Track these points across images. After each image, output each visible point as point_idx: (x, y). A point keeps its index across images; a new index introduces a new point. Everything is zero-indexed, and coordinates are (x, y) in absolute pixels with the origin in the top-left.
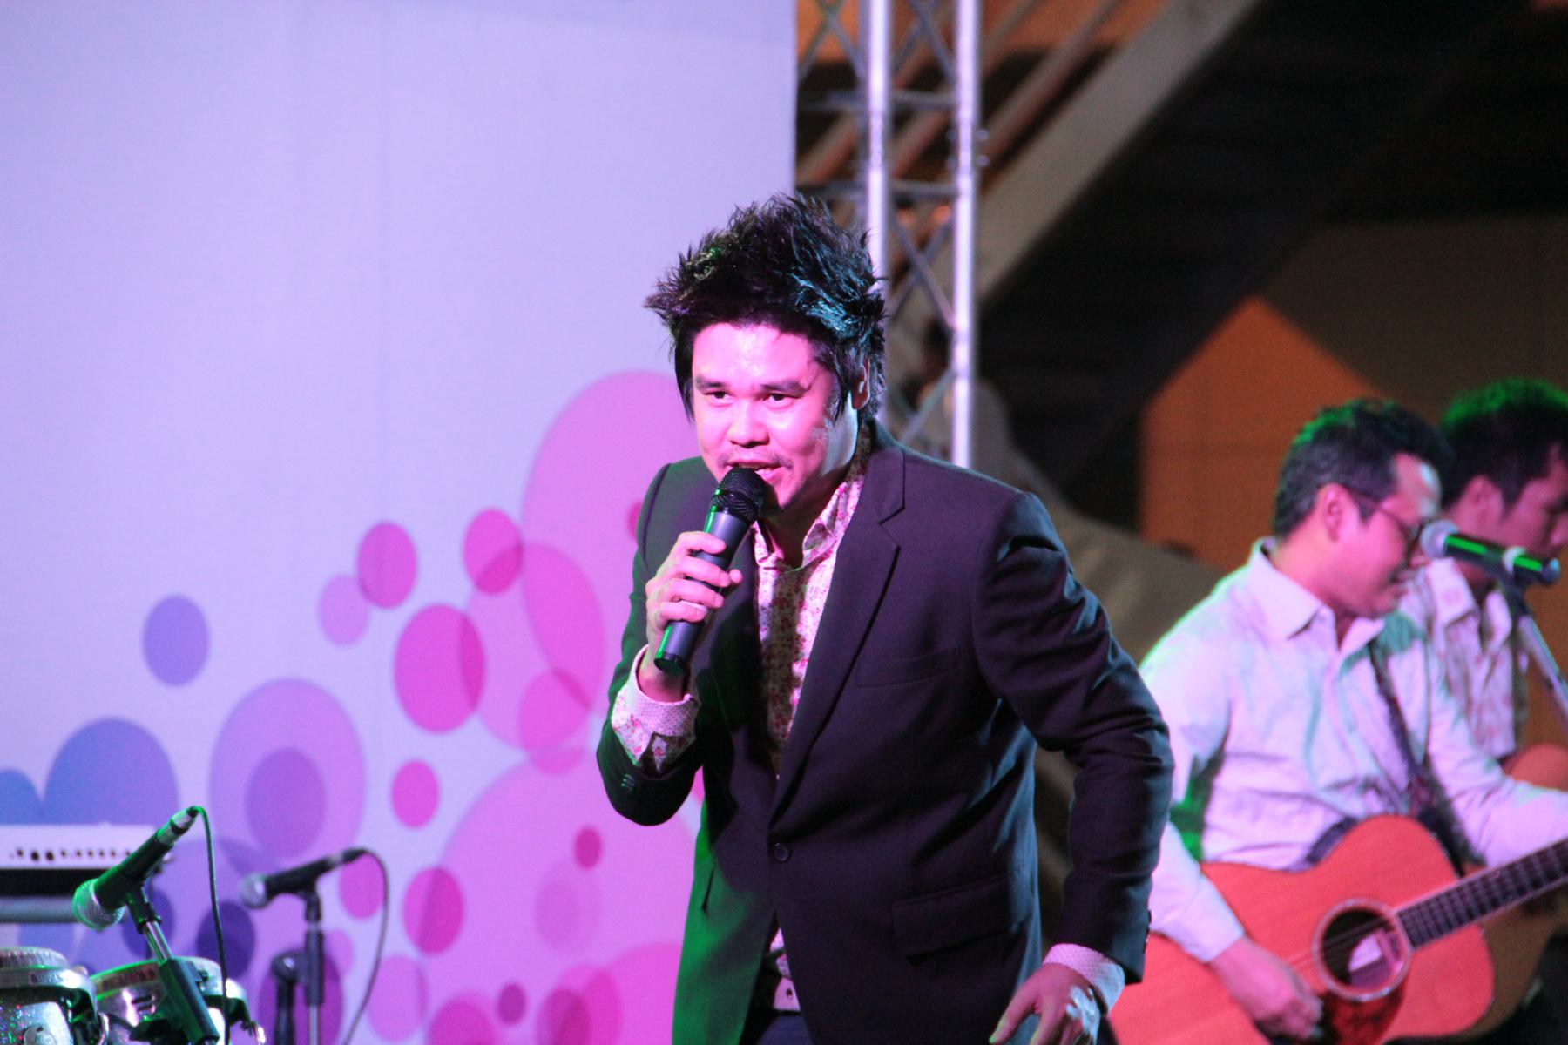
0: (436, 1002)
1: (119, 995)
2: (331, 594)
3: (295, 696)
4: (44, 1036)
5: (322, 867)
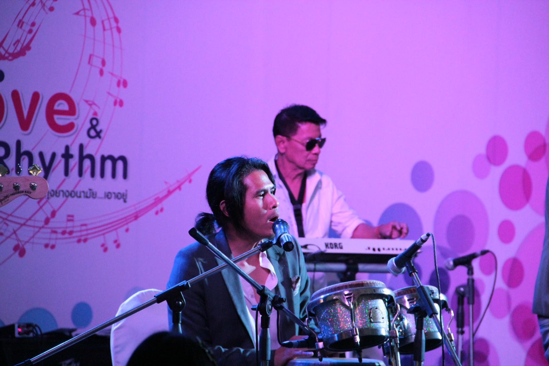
0: (514, 305)
1: (403, 297)
2: (477, 159)
3: (464, 196)
4: (378, 311)
5: (473, 256)
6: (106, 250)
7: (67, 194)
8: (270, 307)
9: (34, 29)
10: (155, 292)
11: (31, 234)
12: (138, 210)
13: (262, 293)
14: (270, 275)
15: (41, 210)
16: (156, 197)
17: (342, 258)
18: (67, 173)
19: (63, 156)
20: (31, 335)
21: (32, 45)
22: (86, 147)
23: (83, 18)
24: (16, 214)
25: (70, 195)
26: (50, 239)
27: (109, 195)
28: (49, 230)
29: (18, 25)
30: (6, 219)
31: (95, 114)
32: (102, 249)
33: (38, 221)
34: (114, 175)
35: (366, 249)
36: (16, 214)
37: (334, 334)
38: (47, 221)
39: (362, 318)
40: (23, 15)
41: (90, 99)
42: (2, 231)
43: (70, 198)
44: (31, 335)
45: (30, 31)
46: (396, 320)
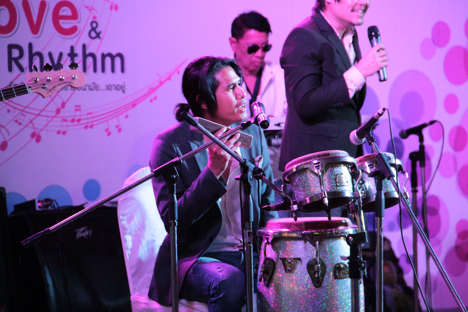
2: (424, 45)
3: (414, 75)
4: (342, 176)
6: (109, 134)
8: (251, 177)
12: (135, 98)
15: (52, 103)
19: (69, 55)
20: (50, 208)
22: (88, 47)
24: (31, 106)
26: (61, 126)
27: (110, 87)
28: (60, 119)
30: (23, 111)
31: (95, 17)
34: (113, 70)
38: (58, 111)
39: (330, 182)
44: (50, 208)
46: (359, 183)
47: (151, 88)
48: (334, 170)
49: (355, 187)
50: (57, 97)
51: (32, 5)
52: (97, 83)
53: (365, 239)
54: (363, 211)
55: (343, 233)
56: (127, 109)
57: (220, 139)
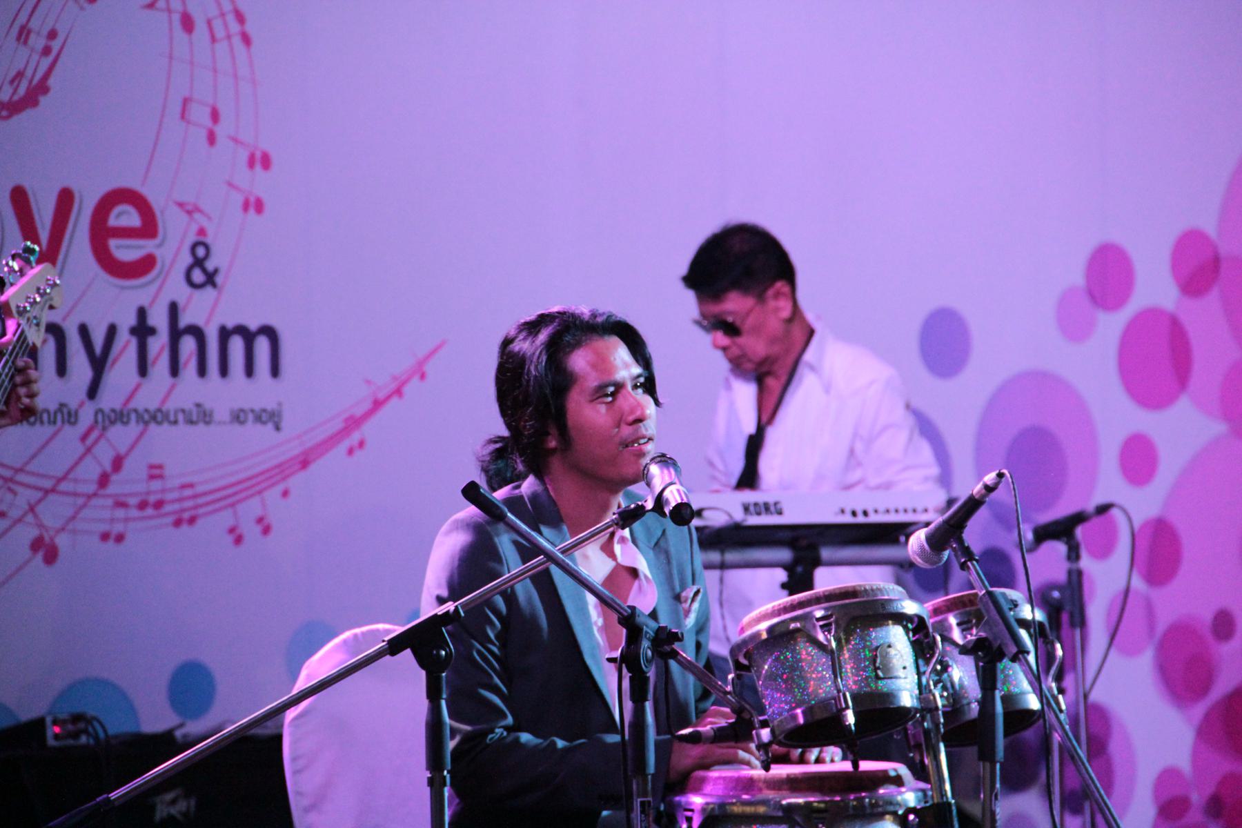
0: (1161, 627)
1: (946, 620)
2: (1065, 303)
3: (1039, 383)
4: (892, 652)
6: (239, 540)
7: (146, 417)
8: (649, 653)
9: (56, 45)
10: (388, 632)
11: (69, 512)
12: (308, 445)
13: (629, 621)
14: (636, 583)
15: (88, 459)
16: (345, 416)
17: (781, 534)
18: (143, 370)
19: (133, 331)
20: (83, 739)
21: (51, 82)
22: (184, 309)
23: (165, 15)
24: (30, 468)
25: (154, 418)
26: (112, 520)
27: (242, 415)
28: (109, 502)
29: (18, 39)
30: (11, 480)
31: (202, 232)
32: (230, 539)
33: (85, 481)
34: (249, 370)
35: (836, 514)
36: (30, 468)
37: (795, 708)
38: (104, 480)
39: (858, 669)
40: (30, 10)
41: (188, 198)
42: (3, 507)
43: (152, 426)
44: (83, 739)
45: (46, 51)
46: (934, 670)
47: (351, 417)
48: (869, 635)
49: (924, 680)
50: (102, 443)
51: (35, 195)
52: (208, 405)
53: (952, 822)
54: (946, 746)
55: (891, 803)
56: (287, 472)
57: (562, 553)
